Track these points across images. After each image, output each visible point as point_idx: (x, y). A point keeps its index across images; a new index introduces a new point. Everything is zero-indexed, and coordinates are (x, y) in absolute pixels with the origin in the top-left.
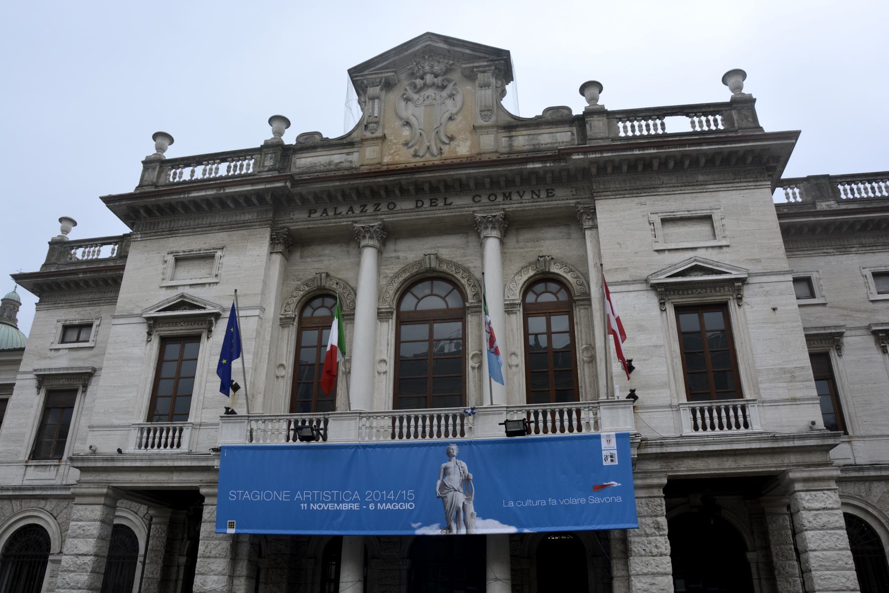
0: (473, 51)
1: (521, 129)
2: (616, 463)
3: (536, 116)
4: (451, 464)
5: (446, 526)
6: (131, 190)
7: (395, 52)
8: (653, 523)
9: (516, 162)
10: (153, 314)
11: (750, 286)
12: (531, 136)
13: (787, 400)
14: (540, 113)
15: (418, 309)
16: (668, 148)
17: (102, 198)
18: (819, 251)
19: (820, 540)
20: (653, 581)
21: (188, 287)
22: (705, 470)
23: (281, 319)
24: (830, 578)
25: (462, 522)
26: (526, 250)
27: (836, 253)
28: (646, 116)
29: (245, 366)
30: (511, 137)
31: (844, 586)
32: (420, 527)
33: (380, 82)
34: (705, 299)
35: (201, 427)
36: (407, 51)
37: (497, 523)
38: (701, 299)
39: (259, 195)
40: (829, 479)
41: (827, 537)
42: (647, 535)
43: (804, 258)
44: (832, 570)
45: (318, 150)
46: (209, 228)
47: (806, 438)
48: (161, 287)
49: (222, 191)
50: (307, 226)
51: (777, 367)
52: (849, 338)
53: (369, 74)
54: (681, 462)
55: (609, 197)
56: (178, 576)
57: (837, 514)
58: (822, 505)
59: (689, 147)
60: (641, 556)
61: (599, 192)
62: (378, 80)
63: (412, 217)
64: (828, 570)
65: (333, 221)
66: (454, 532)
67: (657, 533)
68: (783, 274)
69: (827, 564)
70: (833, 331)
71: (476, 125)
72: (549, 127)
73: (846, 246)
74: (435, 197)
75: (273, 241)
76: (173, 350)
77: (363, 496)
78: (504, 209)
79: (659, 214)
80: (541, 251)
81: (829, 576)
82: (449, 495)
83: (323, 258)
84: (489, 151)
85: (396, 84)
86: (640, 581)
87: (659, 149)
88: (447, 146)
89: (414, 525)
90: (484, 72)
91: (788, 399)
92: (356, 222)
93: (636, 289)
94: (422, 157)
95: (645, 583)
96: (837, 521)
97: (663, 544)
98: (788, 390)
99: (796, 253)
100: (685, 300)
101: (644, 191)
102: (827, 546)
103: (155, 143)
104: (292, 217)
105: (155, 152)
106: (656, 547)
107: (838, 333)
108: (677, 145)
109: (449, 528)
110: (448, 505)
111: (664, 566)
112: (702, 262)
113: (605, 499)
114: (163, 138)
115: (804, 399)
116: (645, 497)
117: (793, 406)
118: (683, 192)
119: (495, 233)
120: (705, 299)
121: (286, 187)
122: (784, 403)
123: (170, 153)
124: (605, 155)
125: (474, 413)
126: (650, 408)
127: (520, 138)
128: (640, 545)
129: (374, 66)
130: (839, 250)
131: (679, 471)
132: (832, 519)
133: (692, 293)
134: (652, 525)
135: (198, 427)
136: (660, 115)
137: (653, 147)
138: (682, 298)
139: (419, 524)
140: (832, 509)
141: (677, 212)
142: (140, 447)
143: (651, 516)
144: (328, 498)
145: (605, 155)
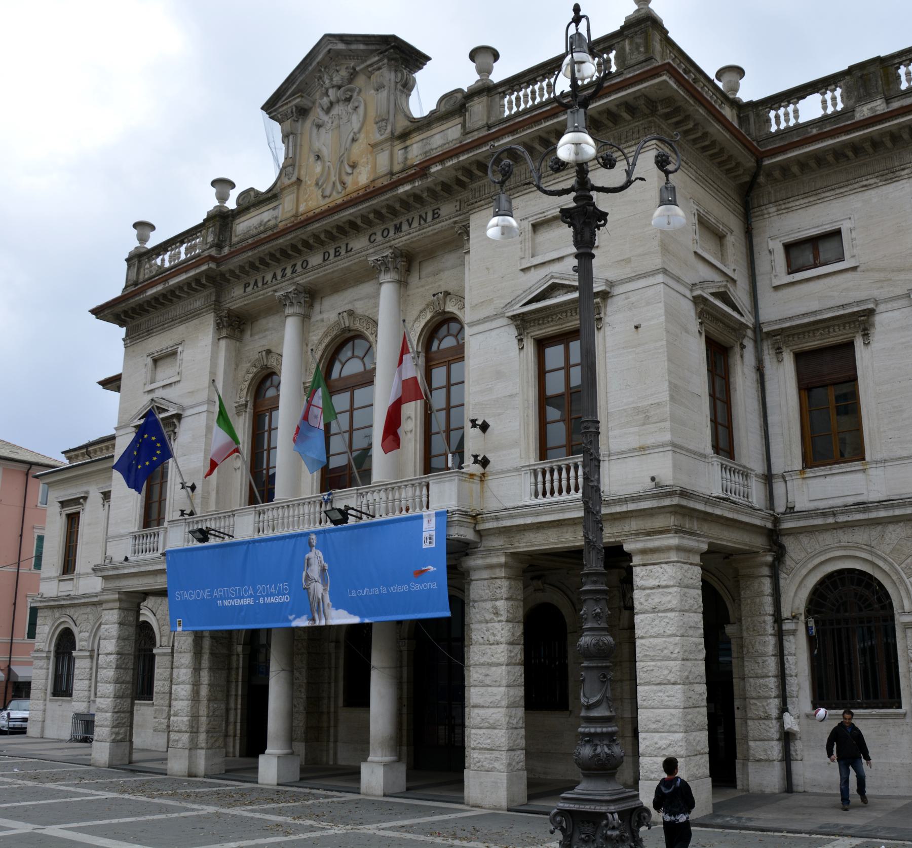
0: (367, 44)
1: (415, 134)
2: (433, 545)
3: (431, 112)
4: (311, 555)
5: (311, 617)
6: (117, 293)
7: (299, 70)
8: (493, 607)
9: (386, 189)
10: (518, 310)
11: (615, 299)
12: (424, 141)
13: (634, 450)
14: (433, 107)
15: (342, 375)
16: (524, 130)
17: (90, 311)
18: (856, 186)
19: (650, 625)
20: (487, 672)
21: (161, 389)
22: (543, 545)
23: (236, 407)
24: (652, 670)
25: (322, 613)
26: (427, 288)
27: (881, 184)
28: (530, 80)
29: (181, 469)
30: (406, 148)
31: (664, 679)
32: (294, 619)
33: (292, 112)
34: (564, 326)
35: (611, 458)
36: (311, 64)
37: (345, 613)
38: (561, 327)
39: (197, 279)
40: (668, 549)
41: (657, 622)
42: (487, 622)
43: (834, 201)
44: (658, 660)
45: (252, 210)
46: (173, 323)
47: (639, 499)
48: (145, 392)
49: (167, 285)
50: (243, 304)
51: (631, 406)
52: (885, 315)
53: (282, 106)
54: (522, 536)
55: (483, 208)
56: (238, 665)
57: (670, 593)
58: (656, 583)
59: (545, 122)
60: (480, 644)
61: (472, 204)
62: (289, 112)
63: (321, 274)
64: (653, 660)
65: (261, 292)
66: (317, 624)
67: (495, 619)
68: (653, 275)
69: (652, 654)
70: (856, 309)
71: (372, 142)
72: (440, 123)
73: (895, 169)
74: (338, 245)
75: (219, 326)
76: (555, 355)
77: (255, 591)
78: (390, 247)
79: (530, 219)
80: (440, 286)
81: (651, 668)
82: (312, 587)
83: (267, 333)
84: (383, 174)
85: (311, 108)
86: (477, 672)
87: (514, 135)
88: (351, 177)
89: (291, 618)
90: (379, 69)
91: (636, 449)
92: (275, 291)
93: (498, 326)
94: (330, 196)
95: (480, 674)
96: (670, 602)
97: (499, 631)
98: (639, 436)
99: (823, 195)
100: (544, 331)
101: (517, 190)
102: (655, 632)
103: (474, 64)
104: (232, 295)
105: (478, 77)
106: (494, 635)
107: (864, 310)
108: (531, 123)
109: (314, 620)
110: (311, 597)
111: (498, 656)
112: (559, 278)
113: (423, 585)
114: (143, 227)
115: (653, 447)
116: (488, 579)
117: (642, 457)
118: (557, 181)
119: (296, 309)
120: (564, 326)
121: (210, 268)
122: (631, 455)
123: (500, 73)
124: (461, 158)
125: (234, 515)
126: (503, 472)
127: (437, 136)
128: (480, 633)
129: (285, 94)
130: (884, 178)
131: (519, 547)
132: (665, 599)
133: (552, 321)
134: (491, 610)
135: (606, 458)
136: (545, 74)
137: (507, 134)
138: (541, 329)
139: (294, 616)
140: (667, 587)
141: (547, 211)
142: (536, 496)
143: (492, 600)
144: (233, 594)
145: (461, 158)
